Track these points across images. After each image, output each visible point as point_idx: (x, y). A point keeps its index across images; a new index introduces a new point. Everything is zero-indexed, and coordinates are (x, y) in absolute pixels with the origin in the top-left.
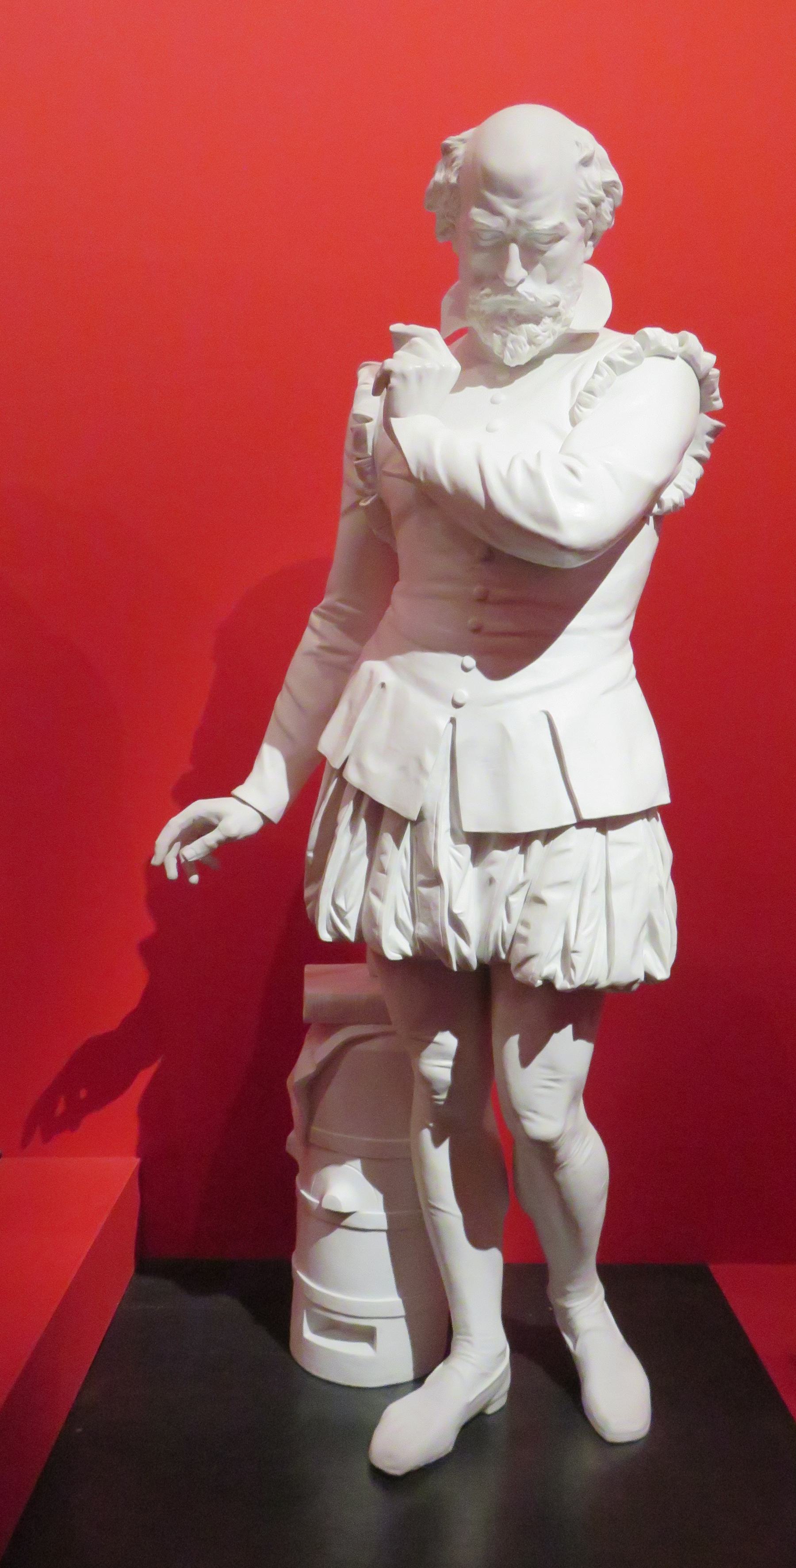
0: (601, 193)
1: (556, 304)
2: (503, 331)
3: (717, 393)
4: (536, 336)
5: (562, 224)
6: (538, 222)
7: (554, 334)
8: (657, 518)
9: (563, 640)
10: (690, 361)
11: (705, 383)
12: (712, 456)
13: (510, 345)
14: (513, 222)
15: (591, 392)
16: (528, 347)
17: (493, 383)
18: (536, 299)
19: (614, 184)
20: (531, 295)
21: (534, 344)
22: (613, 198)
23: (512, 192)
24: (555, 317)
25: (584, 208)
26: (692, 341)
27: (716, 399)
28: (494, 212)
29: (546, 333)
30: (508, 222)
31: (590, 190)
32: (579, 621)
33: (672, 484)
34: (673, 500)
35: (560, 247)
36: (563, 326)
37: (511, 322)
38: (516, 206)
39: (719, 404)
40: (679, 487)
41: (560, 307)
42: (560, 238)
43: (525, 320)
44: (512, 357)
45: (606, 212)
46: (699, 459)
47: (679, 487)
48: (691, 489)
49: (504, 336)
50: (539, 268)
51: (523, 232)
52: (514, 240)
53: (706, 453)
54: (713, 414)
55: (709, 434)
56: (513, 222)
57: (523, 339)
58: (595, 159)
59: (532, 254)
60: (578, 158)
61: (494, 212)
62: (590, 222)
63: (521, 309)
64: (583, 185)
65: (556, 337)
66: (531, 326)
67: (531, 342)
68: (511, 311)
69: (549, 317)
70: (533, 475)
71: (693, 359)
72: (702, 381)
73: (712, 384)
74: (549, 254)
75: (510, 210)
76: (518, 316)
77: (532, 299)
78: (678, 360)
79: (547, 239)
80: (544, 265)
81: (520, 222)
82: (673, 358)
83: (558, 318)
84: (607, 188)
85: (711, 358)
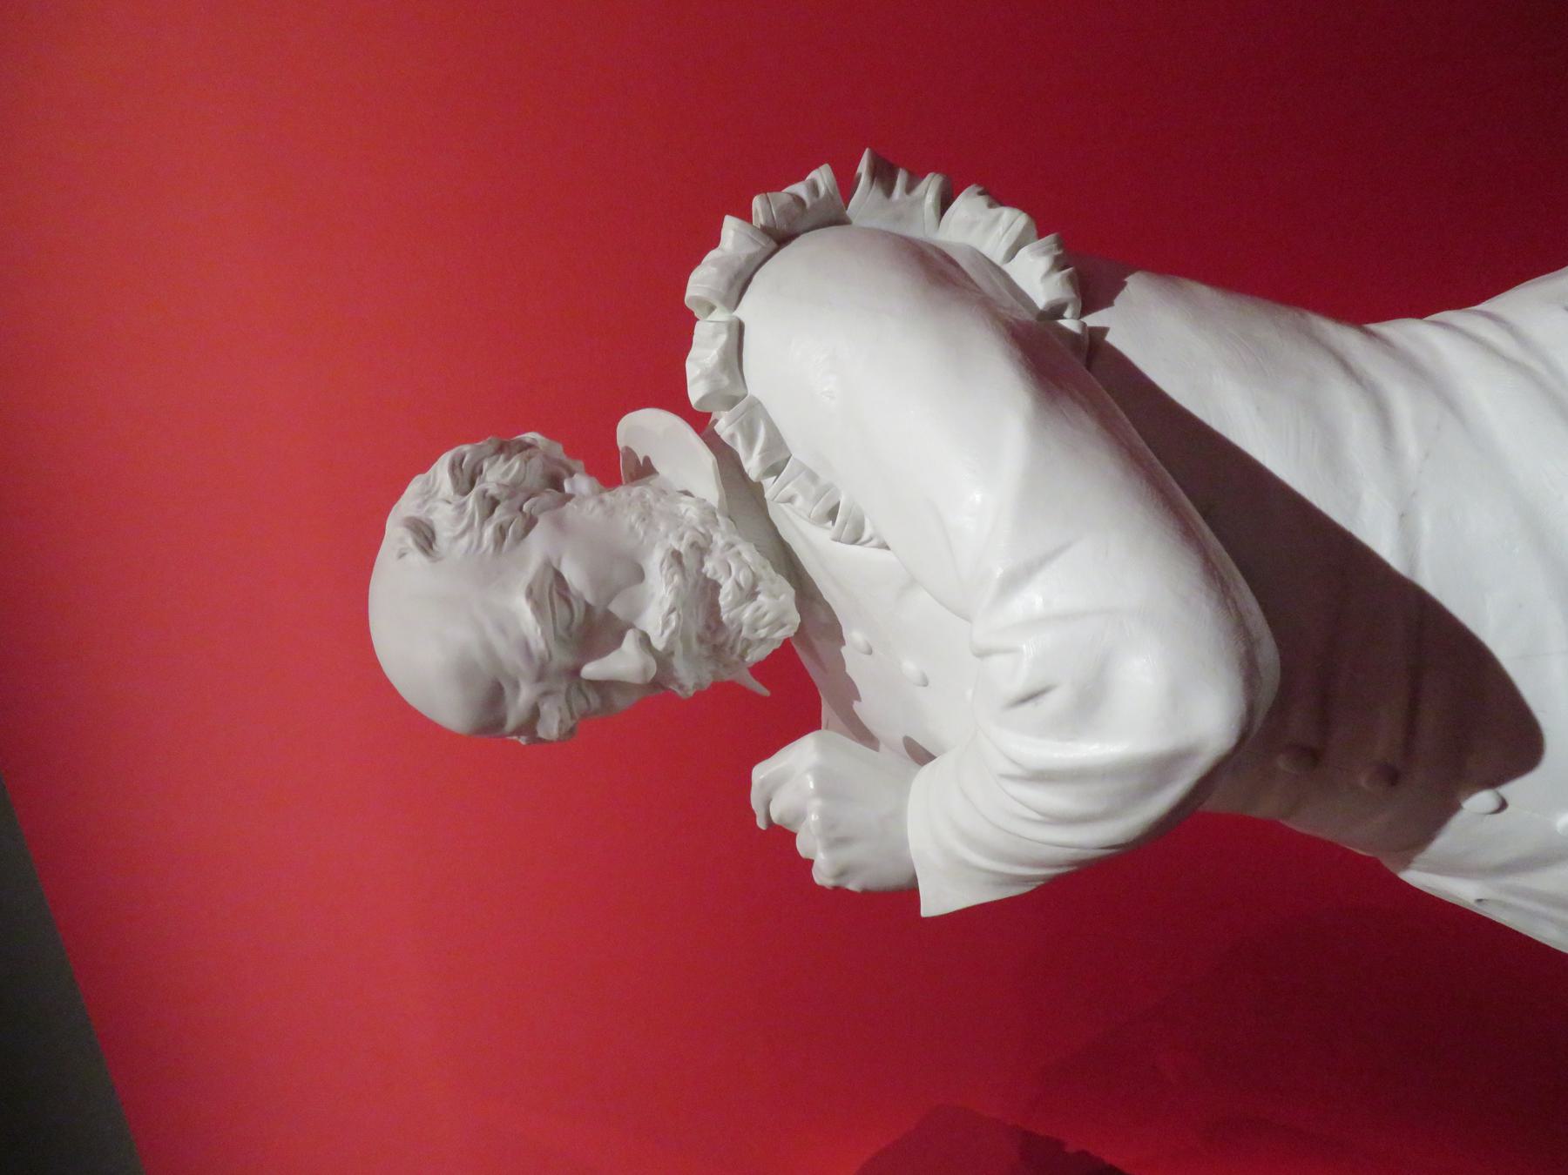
0: (471, 499)
1: (676, 556)
2: (739, 648)
3: (800, 189)
4: (738, 584)
5: (530, 593)
6: (533, 645)
7: (731, 545)
8: (1087, 308)
9: (1429, 581)
10: (740, 283)
11: (783, 226)
12: (936, 170)
13: (762, 633)
14: (541, 688)
15: (832, 514)
16: (761, 598)
17: (834, 632)
18: (672, 611)
19: (455, 467)
20: (666, 623)
21: (754, 585)
22: (481, 460)
23: (495, 696)
24: (701, 549)
25: (502, 532)
26: (702, 282)
27: (814, 188)
28: (535, 713)
29: (734, 563)
30: (545, 694)
31: (470, 526)
32: (1379, 536)
33: (1007, 268)
34: (1047, 274)
35: (573, 574)
36: (717, 522)
37: (721, 639)
38: (516, 686)
39: (822, 176)
40: (1012, 253)
41: (682, 547)
42: (558, 576)
43: (714, 609)
44: (783, 625)
45: (506, 473)
46: (945, 202)
47: (1012, 253)
48: (1012, 220)
49: (749, 644)
50: (617, 608)
51: (562, 658)
52: (575, 672)
53: (930, 187)
54: (846, 185)
55: (889, 192)
56: (541, 688)
57: (747, 613)
58: (420, 514)
59: (594, 630)
60: (416, 558)
61: (535, 713)
62: (525, 508)
63: (696, 627)
64: (464, 542)
65: (736, 538)
66: (725, 598)
67: (753, 595)
68: (701, 640)
69: (702, 564)
70: (1043, 777)
71: (737, 275)
72: (780, 237)
73: (784, 211)
74: (589, 598)
75: (523, 697)
76: (708, 627)
77: (673, 616)
78: (745, 311)
79: (562, 612)
80: (610, 599)
81: (541, 676)
82: (741, 328)
83: (701, 542)
84: (467, 479)
85: (731, 227)
